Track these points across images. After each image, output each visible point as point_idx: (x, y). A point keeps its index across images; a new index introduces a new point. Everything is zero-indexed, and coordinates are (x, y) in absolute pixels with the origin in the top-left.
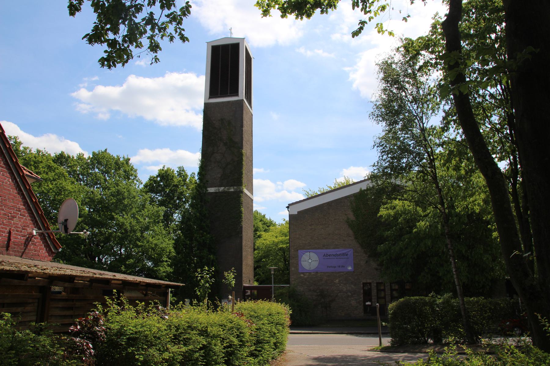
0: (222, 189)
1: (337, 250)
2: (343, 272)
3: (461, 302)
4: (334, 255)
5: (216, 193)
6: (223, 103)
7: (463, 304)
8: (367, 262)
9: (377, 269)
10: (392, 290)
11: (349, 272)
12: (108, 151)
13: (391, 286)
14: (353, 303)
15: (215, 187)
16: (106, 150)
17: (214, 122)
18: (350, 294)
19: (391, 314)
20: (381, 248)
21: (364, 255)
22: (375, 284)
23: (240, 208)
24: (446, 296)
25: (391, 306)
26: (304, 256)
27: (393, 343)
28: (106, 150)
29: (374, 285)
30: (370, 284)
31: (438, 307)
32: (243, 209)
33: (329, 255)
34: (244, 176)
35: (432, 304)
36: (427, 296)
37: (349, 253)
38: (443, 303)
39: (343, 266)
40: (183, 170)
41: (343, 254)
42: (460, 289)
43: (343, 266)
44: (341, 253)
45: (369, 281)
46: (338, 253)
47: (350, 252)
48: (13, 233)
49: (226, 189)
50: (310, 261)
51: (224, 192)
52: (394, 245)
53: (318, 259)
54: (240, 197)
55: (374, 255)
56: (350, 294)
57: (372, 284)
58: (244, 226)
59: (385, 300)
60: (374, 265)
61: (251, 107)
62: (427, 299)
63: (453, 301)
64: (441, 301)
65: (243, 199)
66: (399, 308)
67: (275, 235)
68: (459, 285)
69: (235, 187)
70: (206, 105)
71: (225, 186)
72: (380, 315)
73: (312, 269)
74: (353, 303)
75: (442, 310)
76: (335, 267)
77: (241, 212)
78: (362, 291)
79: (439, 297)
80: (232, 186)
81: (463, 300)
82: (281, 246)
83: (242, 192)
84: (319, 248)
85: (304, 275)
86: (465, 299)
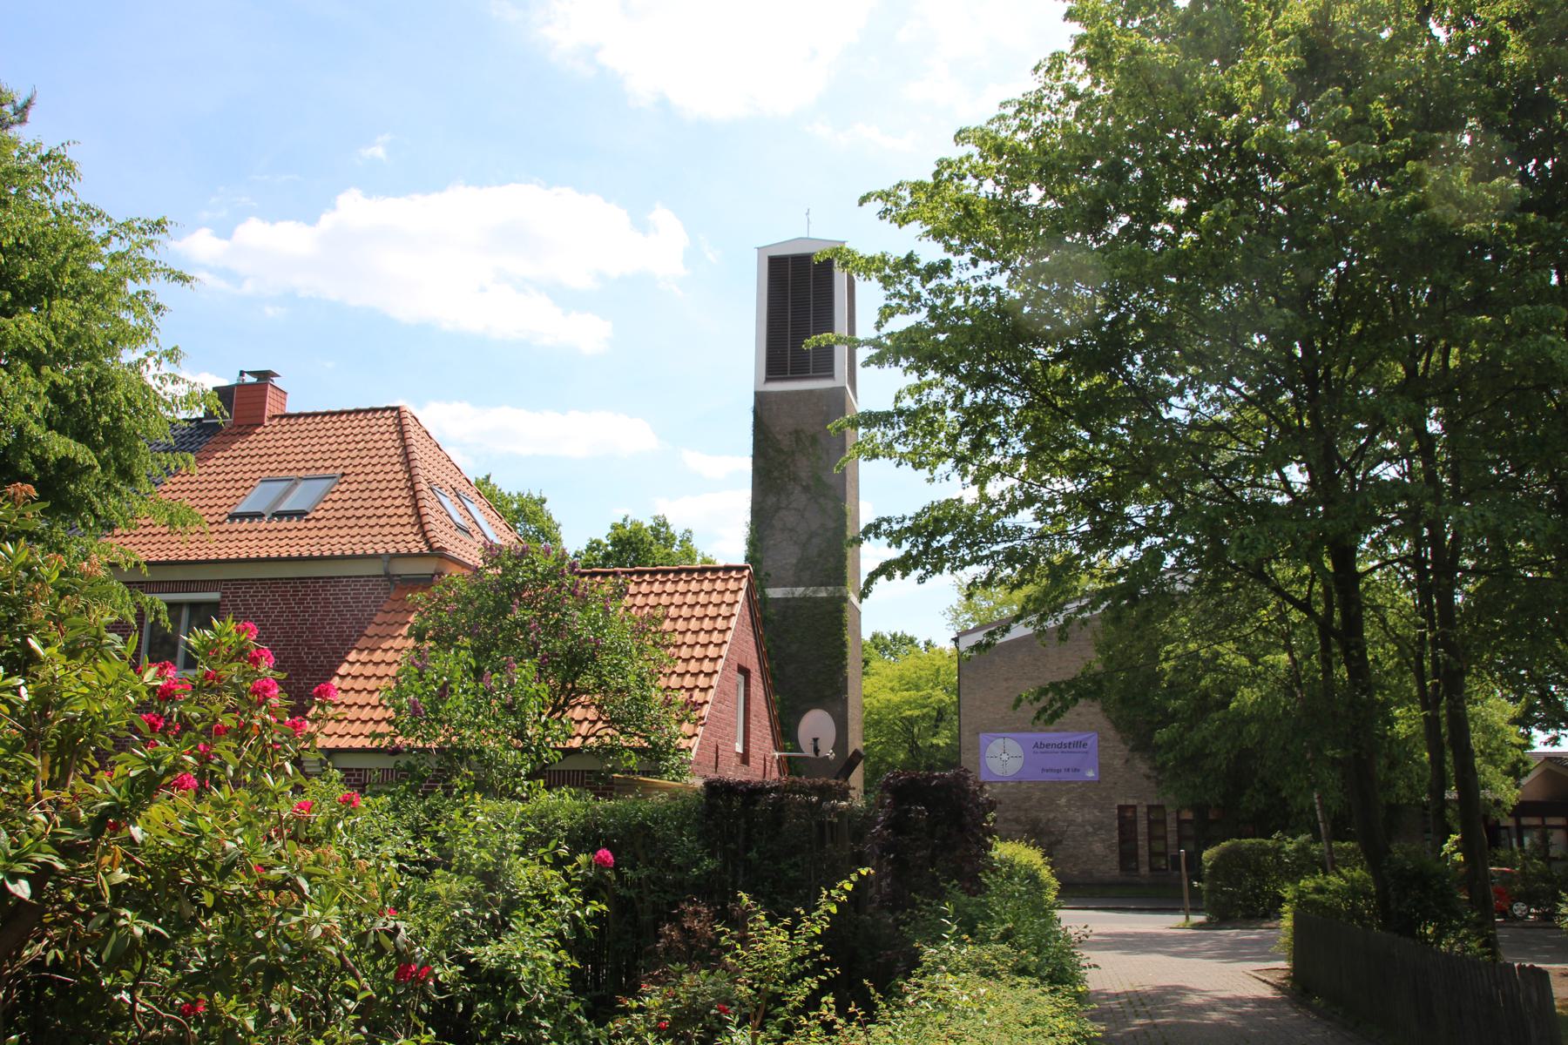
0: (799, 591)
1: (1063, 734)
2: (1076, 782)
3: (1327, 850)
4: (1056, 746)
5: (787, 600)
6: (798, 393)
7: (1331, 853)
8: (1127, 761)
9: (1148, 777)
10: (1180, 822)
11: (1089, 782)
12: (492, 481)
13: (1178, 812)
14: (1098, 848)
15: (785, 586)
16: (488, 477)
17: (779, 437)
18: (1091, 830)
19: (1210, 868)
20: (1162, 735)
21: (1122, 746)
22: (1145, 810)
23: (843, 635)
24: (1302, 838)
25: (1208, 854)
26: (991, 745)
27: (1209, 919)
28: (488, 477)
29: (1142, 811)
30: (1134, 807)
31: (1287, 857)
32: (848, 637)
33: (1047, 746)
34: (849, 563)
35: (1278, 851)
36: (1269, 837)
37: (1089, 742)
38: (1297, 850)
39: (1076, 770)
40: (665, 524)
41: (1077, 744)
42: (1325, 827)
43: (1076, 770)
44: (1071, 740)
45: (1131, 802)
46: (1066, 741)
47: (1092, 739)
48: (720, 747)
49: (810, 592)
50: (1005, 757)
51: (805, 599)
52: (1191, 728)
53: (1022, 754)
54: (841, 611)
55: (1142, 744)
56: (1091, 830)
57: (1139, 809)
58: (850, 675)
59: (1166, 845)
60: (1143, 767)
61: (856, 397)
62: (1269, 843)
63: (1313, 847)
64: (1292, 847)
65: (848, 616)
66: (1223, 857)
67: (889, 685)
68: (1324, 821)
69: (830, 588)
70: (761, 400)
71: (807, 586)
72: (1187, 870)
73: (1009, 774)
74: (1098, 848)
75: (1293, 862)
76: (1059, 771)
77: (844, 644)
78: (1116, 823)
79: (1289, 840)
80: (822, 585)
81: (1330, 847)
82: (909, 713)
83: (845, 599)
84: (1023, 730)
85: (993, 787)
86: (1334, 845)
